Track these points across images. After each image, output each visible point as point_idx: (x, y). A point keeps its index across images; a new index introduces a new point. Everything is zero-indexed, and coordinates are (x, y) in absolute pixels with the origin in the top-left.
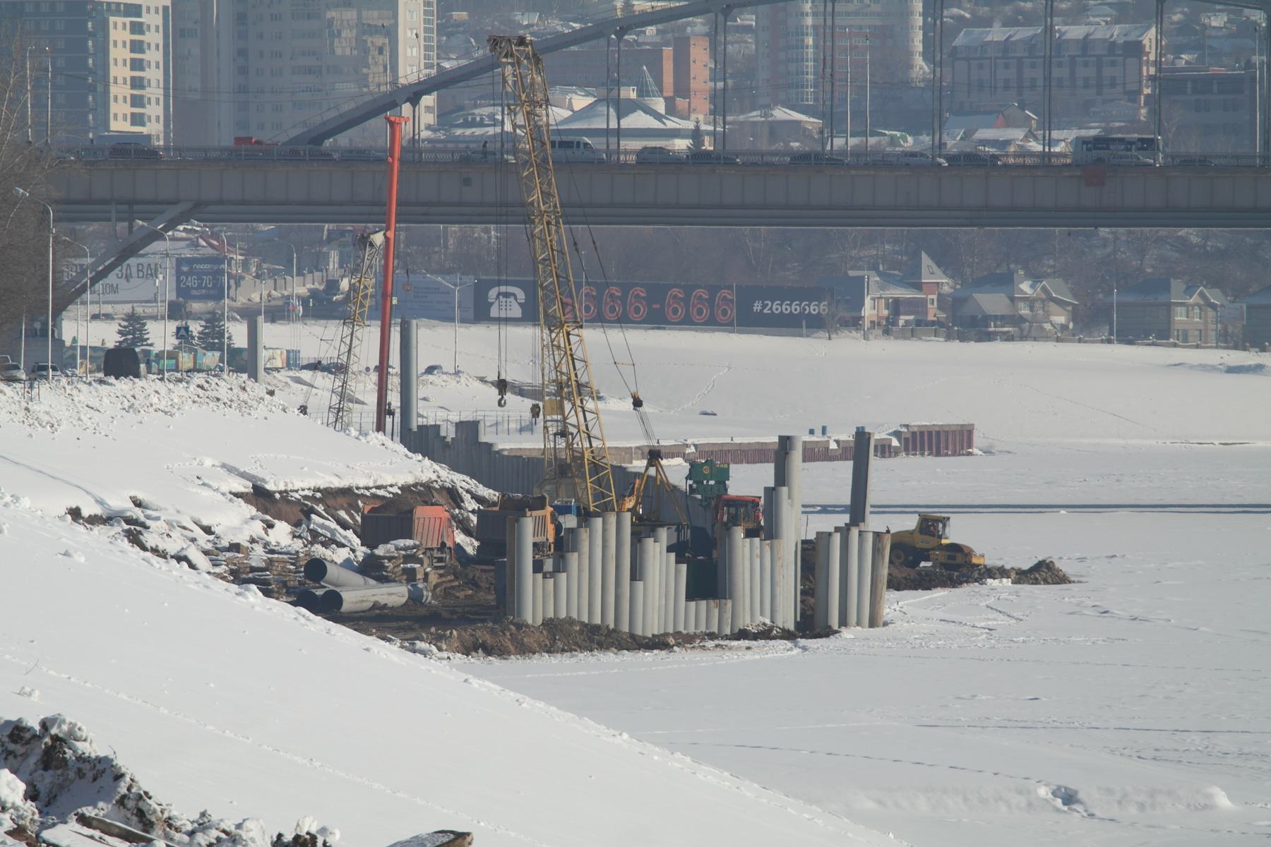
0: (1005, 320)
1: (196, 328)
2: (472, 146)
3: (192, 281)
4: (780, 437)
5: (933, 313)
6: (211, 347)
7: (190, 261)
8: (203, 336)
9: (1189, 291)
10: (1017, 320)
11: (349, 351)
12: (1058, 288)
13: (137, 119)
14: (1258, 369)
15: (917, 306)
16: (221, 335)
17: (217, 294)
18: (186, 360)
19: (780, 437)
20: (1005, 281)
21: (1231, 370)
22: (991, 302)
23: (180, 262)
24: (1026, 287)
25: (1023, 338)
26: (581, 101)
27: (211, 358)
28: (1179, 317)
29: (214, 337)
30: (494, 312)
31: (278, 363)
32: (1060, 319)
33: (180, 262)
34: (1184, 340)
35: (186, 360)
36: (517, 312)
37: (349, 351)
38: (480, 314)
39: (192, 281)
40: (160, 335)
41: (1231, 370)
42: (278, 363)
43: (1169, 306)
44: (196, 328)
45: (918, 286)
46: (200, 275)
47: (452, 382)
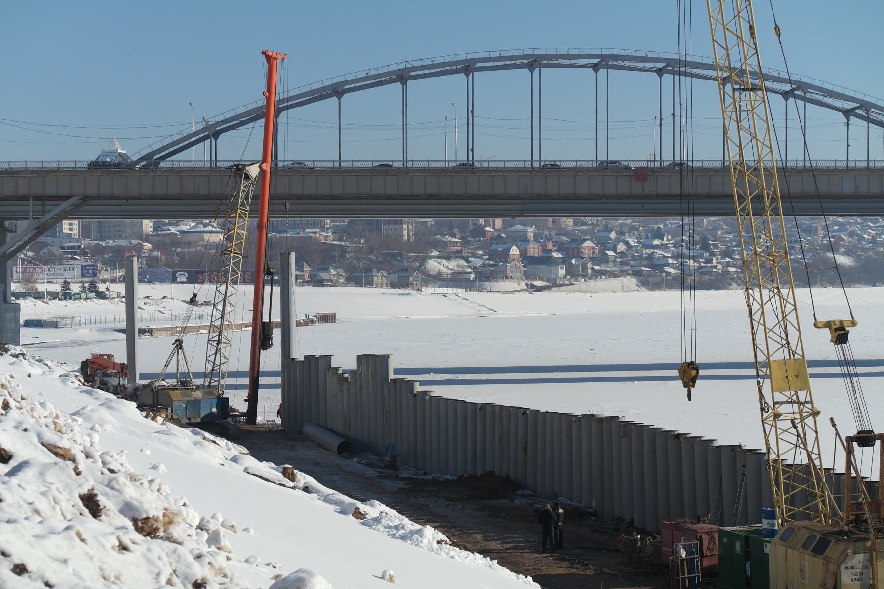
0: (328, 280)
1: (87, 285)
2: (79, 165)
3: (86, 272)
4: (359, 358)
5: (307, 279)
6: (92, 291)
7: (85, 266)
8: (90, 288)
9: (378, 272)
10: (331, 281)
11: (225, 300)
12: (341, 271)
13: (71, 229)
14: (409, 294)
15: (302, 277)
16: (95, 287)
17: (95, 275)
18: (83, 295)
19: (359, 358)
20: (326, 270)
21: (400, 295)
22: (324, 275)
23: (82, 266)
24: (332, 271)
25: (334, 286)
26: (193, 224)
27: (93, 294)
28: (375, 279)
29: (93, 288)
30: (179, 280)
31: (115, 296)
32: (342, 281)
33: (82, 266)
34: (377, 286)
35: (83, 295)
36: (185, 280)
37: (225, 300)
38: (175, 280)
39: (86, 272)
40: (75, 288)
41: (400, 295)
42: (115, 296)
43: (372, 277)
44: (87, 285)
45: (303, 271)
46: (88, 270)
47: (172, 301)
